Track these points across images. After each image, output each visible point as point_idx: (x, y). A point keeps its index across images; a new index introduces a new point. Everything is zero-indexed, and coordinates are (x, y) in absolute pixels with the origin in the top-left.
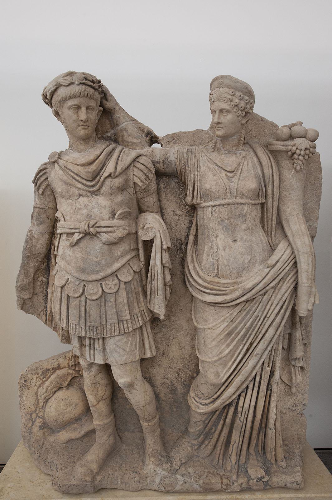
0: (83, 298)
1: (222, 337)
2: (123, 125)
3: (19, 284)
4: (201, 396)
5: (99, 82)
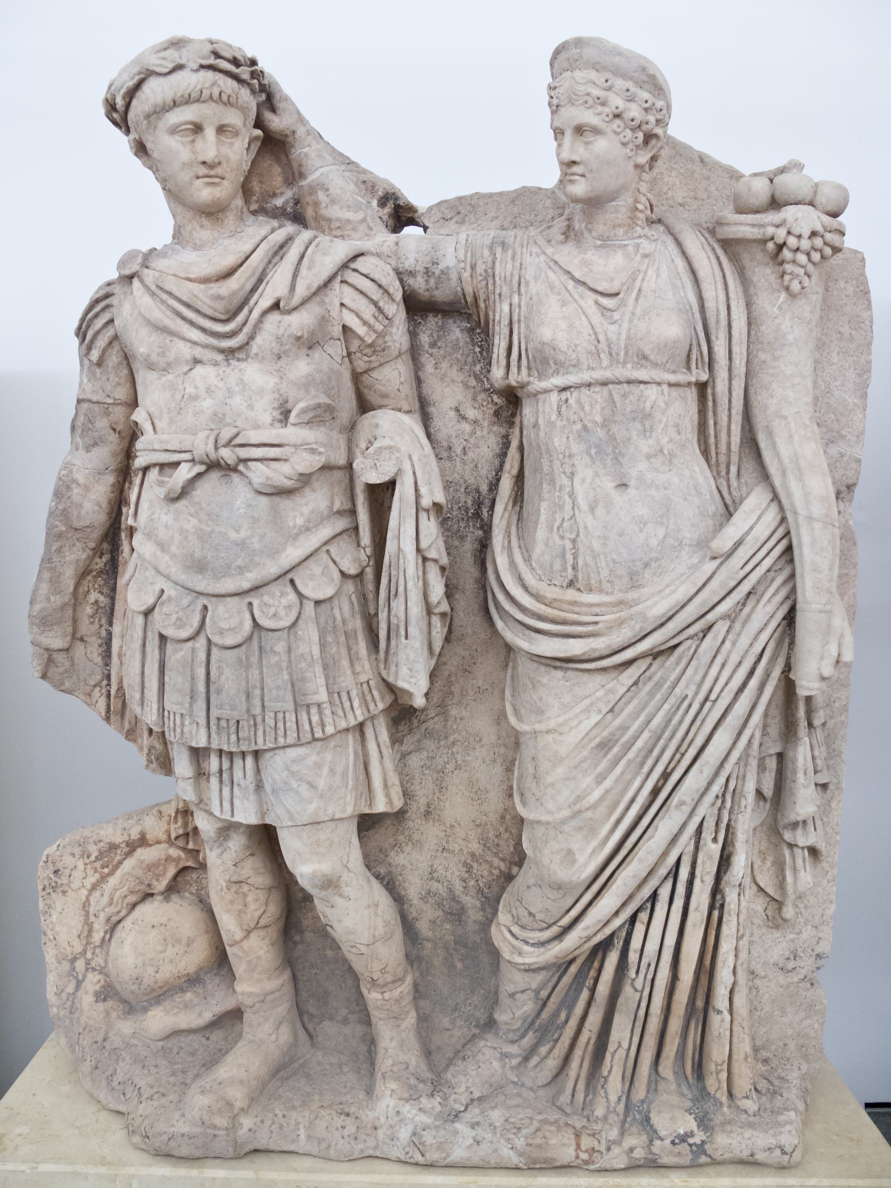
0: (201, 643)
3: (37, 607)
4: (526, 920)
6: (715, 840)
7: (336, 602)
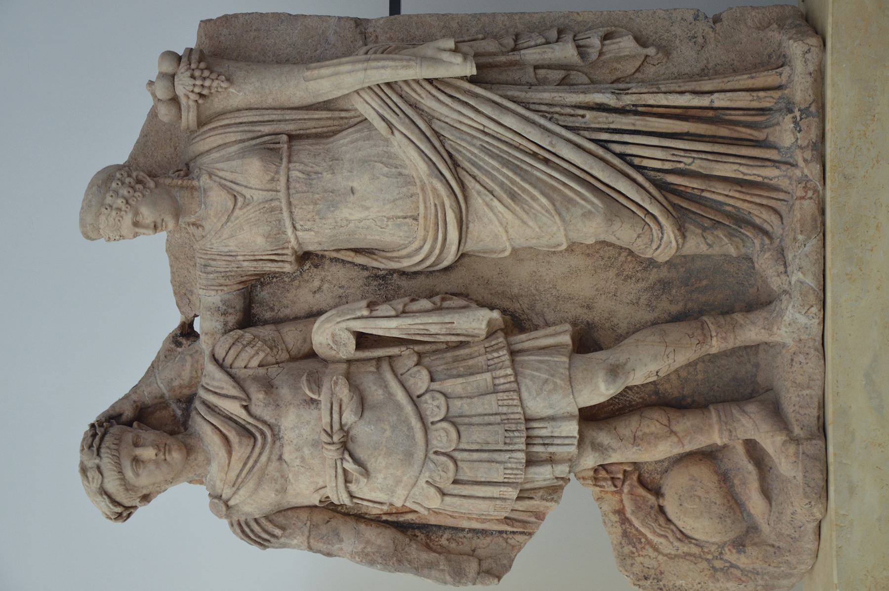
1: (518, 209)
2: (161, 386)
3: (448, 578)
5: (93, 426)
6: (583, 116)
7: (433, 369)
